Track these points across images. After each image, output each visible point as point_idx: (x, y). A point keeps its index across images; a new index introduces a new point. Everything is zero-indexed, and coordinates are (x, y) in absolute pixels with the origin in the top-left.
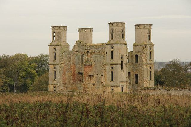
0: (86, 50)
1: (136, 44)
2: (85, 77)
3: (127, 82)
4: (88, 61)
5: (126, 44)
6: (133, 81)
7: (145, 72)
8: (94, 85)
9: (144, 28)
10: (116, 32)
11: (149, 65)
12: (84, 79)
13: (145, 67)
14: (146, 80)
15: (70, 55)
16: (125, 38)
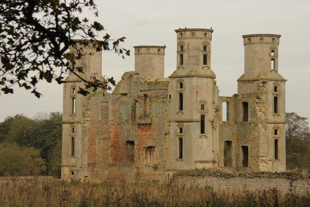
0: (141, 91)
1: (246, 78)
2: (139, 150)
3: (214, 162)
4: (145, 115)
5: (213, 77)
6: (237, 160)
7: (262, 140)
8: (156, 168)
9: (262, 43)
10: (189, 49)
11: (271, 126)
12: (136, 156)
13: (263, 130)
14: (264, 158)
15: (107, 102)
16: (212, 63)
